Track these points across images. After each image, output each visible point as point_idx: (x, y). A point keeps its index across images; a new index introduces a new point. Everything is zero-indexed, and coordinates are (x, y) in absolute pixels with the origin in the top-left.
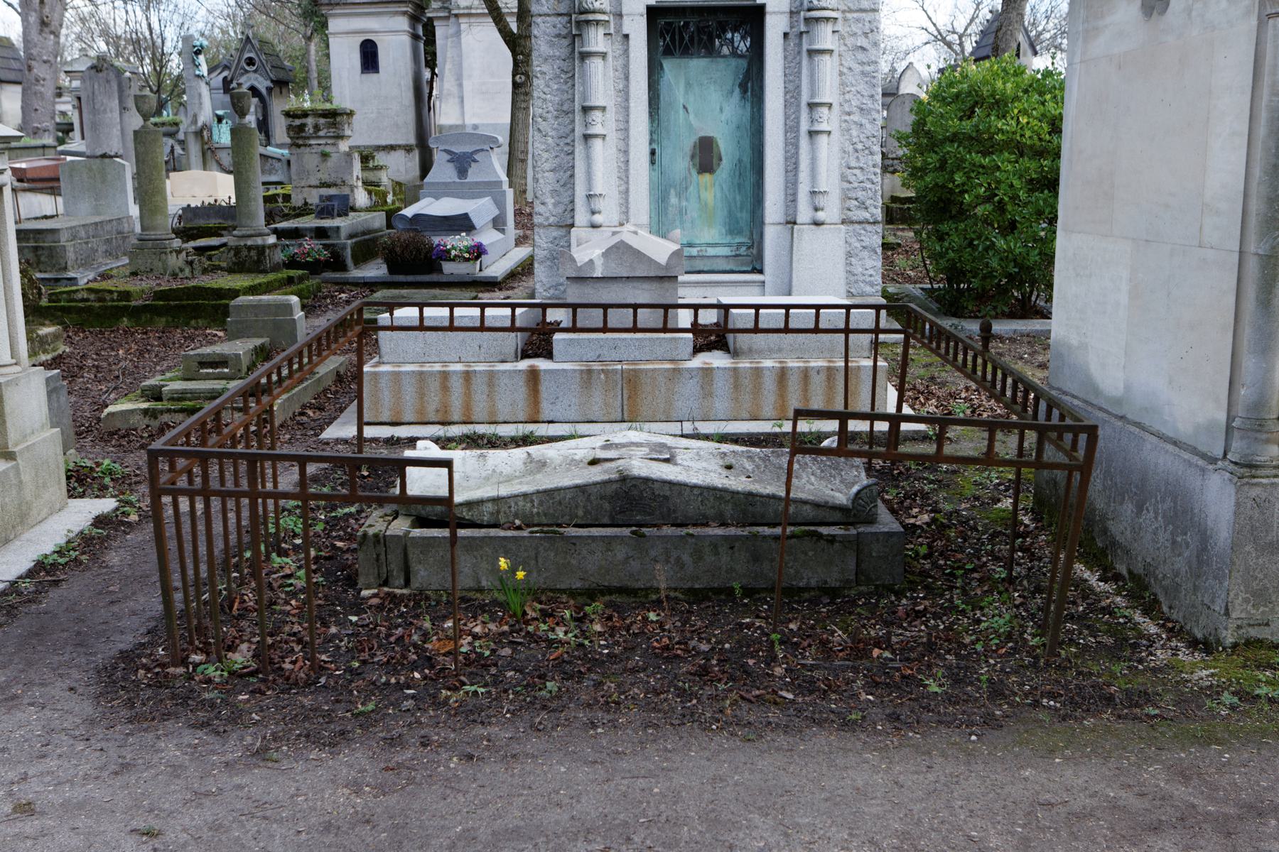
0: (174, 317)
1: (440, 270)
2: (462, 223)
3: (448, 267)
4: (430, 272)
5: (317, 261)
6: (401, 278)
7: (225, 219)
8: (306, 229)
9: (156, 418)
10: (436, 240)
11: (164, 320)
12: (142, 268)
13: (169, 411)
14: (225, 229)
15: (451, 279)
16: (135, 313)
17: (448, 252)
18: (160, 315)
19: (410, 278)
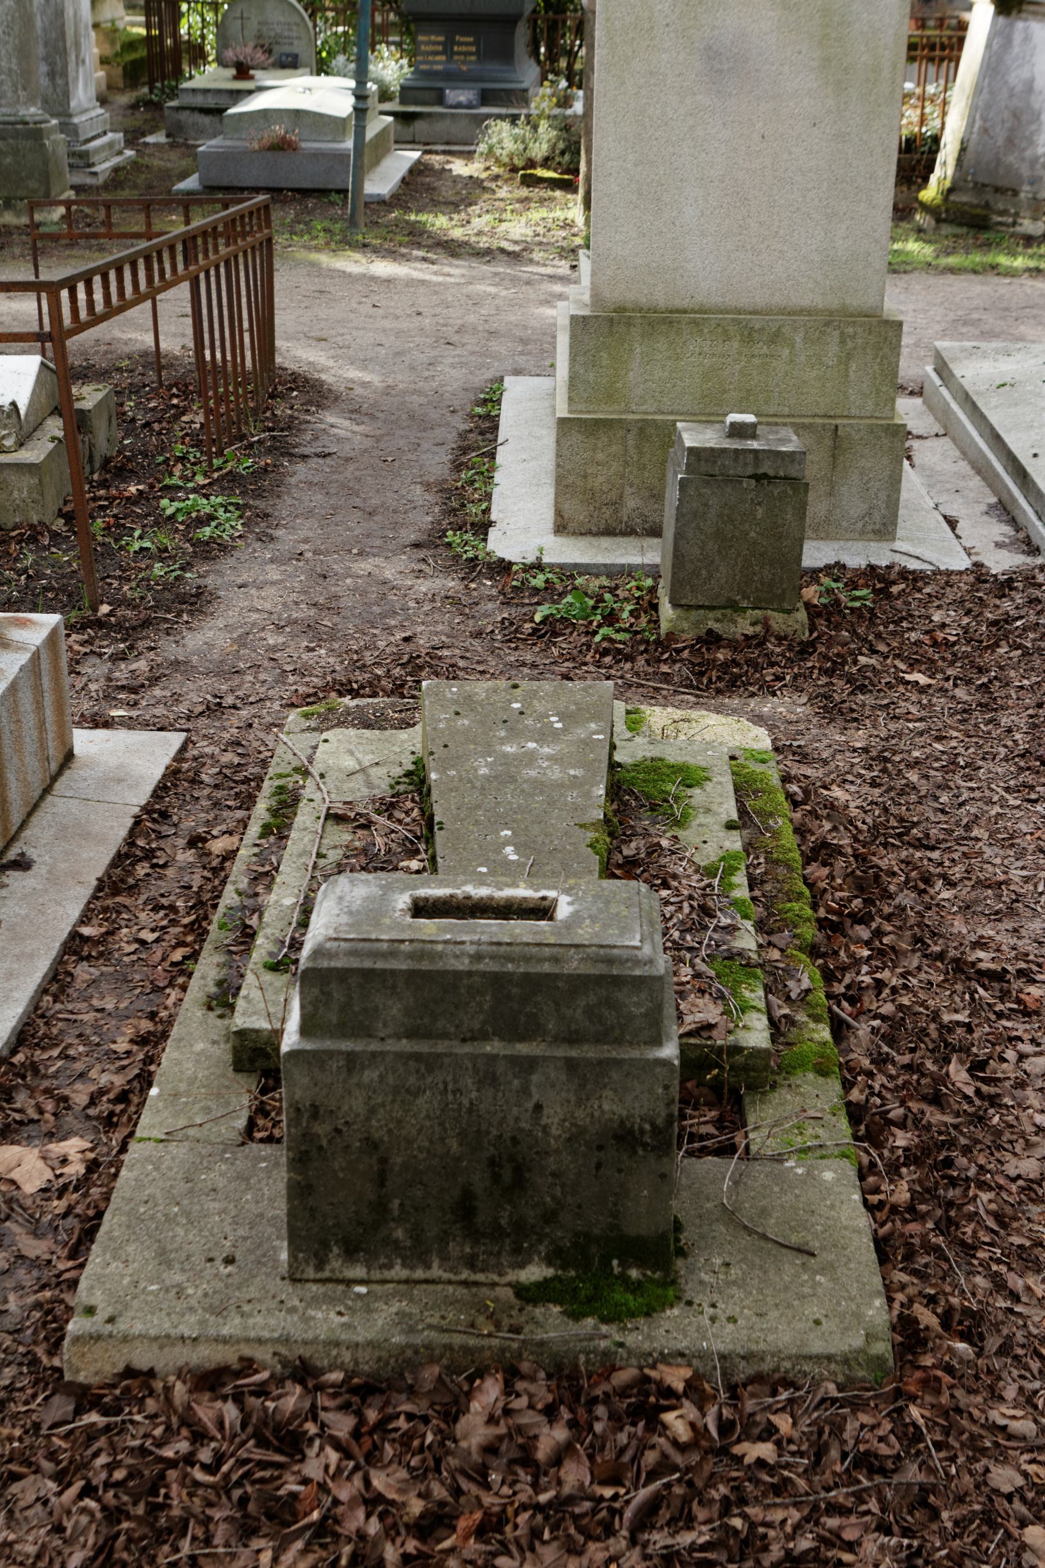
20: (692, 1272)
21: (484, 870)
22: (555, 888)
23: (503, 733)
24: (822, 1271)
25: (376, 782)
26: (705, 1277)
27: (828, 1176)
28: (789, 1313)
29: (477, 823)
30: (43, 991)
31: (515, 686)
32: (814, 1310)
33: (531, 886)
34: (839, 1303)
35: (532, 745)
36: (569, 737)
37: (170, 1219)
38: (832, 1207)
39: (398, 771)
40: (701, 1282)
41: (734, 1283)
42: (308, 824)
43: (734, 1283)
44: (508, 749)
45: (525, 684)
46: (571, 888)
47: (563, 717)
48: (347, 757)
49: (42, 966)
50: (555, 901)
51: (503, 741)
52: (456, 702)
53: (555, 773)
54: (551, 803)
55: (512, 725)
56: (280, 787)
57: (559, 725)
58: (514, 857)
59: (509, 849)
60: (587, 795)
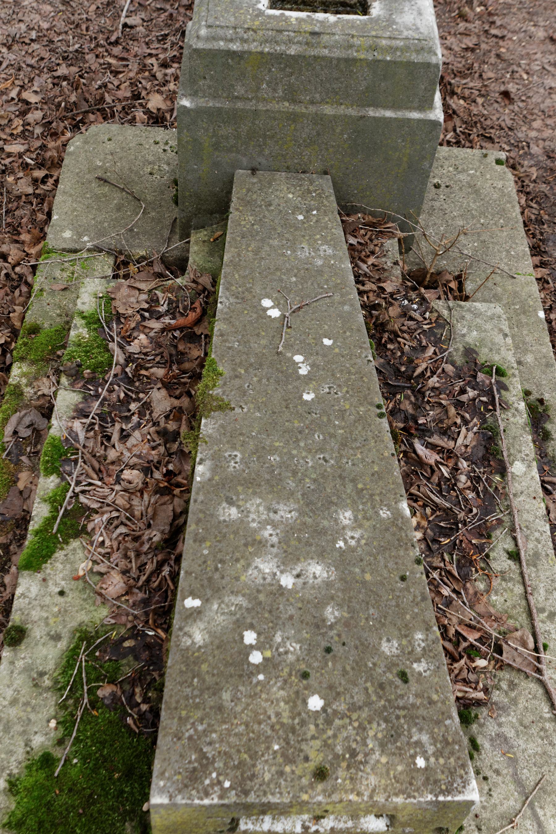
20: (173, 170)
21: (327, 342)
22: (270, 17)
24: (97, 168)
26: (166, 167)
28: (124, 145)
32: (109, 146)
33: (287, 18)
34: (94, 149)
37: (482, 214)
38: (75, 210)
40: (169, 164)
41: (150, 163)
43: (150, 163)
46: (257, 16)
50: (271, 8)
58: (298, 358)
59: (304, 371)
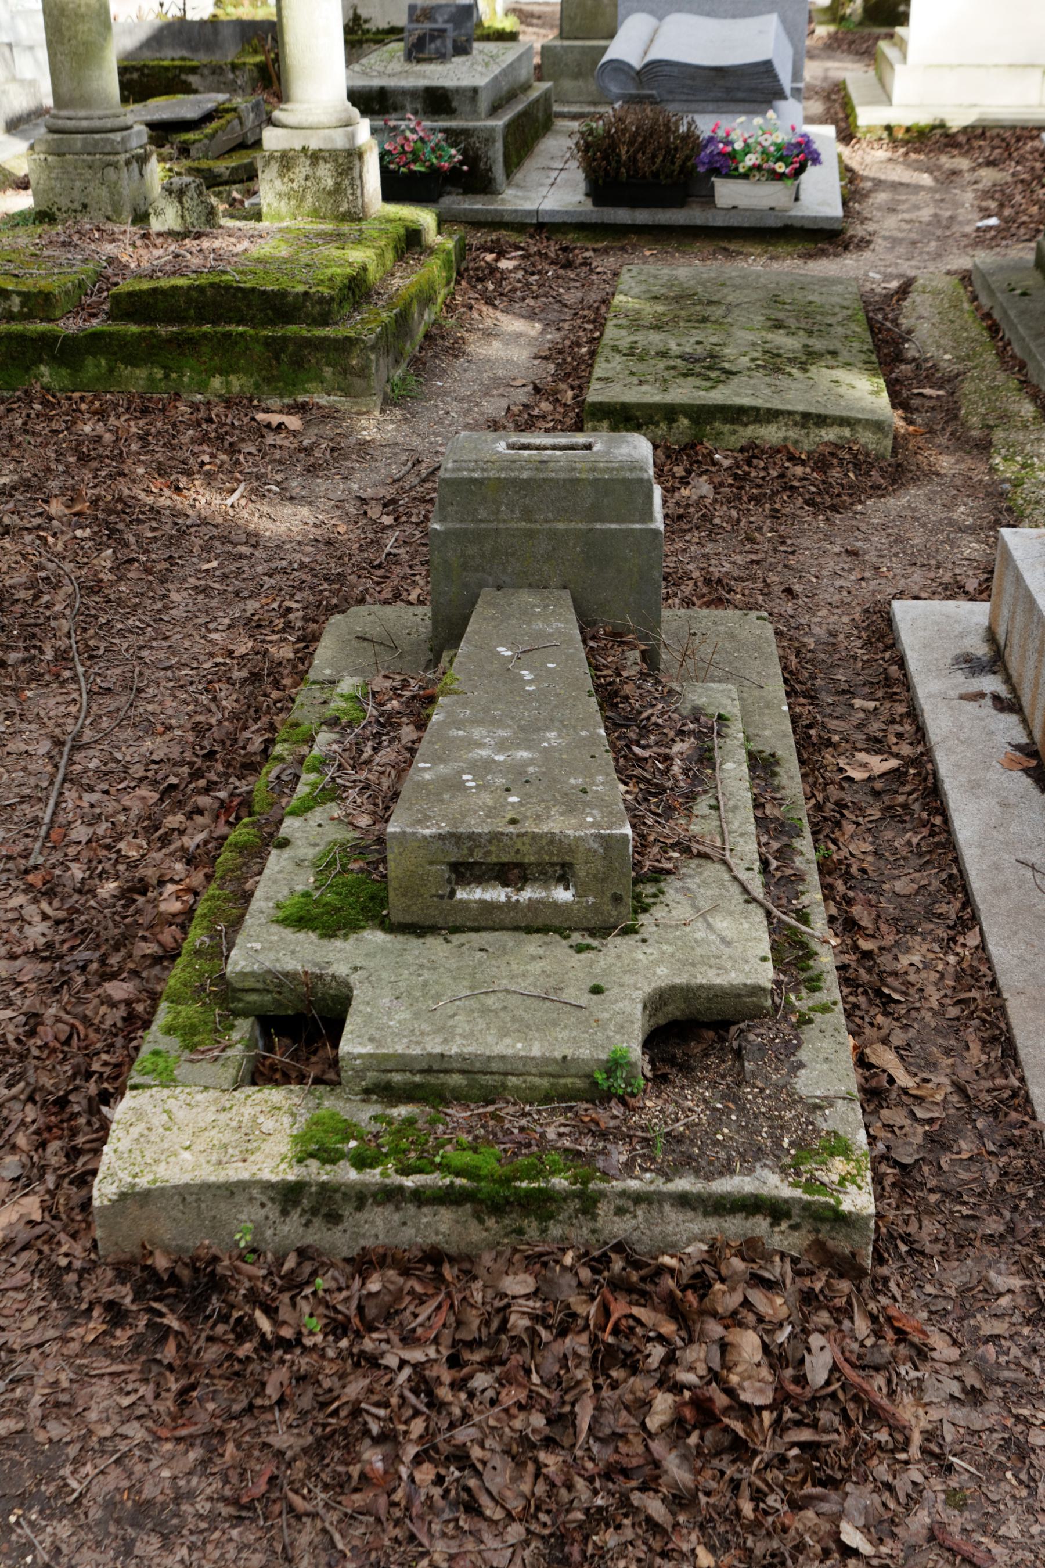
0: (167, 369)
1: (709, 198)
2: (752, 86)
3: (728, 193)
4: (680, 202)
5: (434, 172)
6: (622, 215)
7: (194, 49)
8: (404, 92)
9: (334, 1218)
10: (705, 124)
11: (141, 373)
12: (64, 202)
13: (391, 1195)
14: (193, 70)
15: (735, 221)
16: (68, 352)
17: (733, 156)
18: (132, 361)
19: (642, 216)
23: (531, 769)
25: (680, 897)
27: (328, 672)
29: (557, 695)
30: (962, 873)
31: (513, 822)
35: (500, 758)
36: (456, 765)
39: (659, 912)
42: (741, 840)
44: (525, 754)
45: (502, 827)
47: (461, 786)
48: (728, 934)
49: (978, 884)
51: (531, 762)
52: (587, 804)
53: (478, 732)
54: (486, 710)
55: (520, 777)
56: (814, 990)
57: (465, 777)
60: (449, 714)
